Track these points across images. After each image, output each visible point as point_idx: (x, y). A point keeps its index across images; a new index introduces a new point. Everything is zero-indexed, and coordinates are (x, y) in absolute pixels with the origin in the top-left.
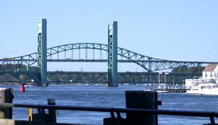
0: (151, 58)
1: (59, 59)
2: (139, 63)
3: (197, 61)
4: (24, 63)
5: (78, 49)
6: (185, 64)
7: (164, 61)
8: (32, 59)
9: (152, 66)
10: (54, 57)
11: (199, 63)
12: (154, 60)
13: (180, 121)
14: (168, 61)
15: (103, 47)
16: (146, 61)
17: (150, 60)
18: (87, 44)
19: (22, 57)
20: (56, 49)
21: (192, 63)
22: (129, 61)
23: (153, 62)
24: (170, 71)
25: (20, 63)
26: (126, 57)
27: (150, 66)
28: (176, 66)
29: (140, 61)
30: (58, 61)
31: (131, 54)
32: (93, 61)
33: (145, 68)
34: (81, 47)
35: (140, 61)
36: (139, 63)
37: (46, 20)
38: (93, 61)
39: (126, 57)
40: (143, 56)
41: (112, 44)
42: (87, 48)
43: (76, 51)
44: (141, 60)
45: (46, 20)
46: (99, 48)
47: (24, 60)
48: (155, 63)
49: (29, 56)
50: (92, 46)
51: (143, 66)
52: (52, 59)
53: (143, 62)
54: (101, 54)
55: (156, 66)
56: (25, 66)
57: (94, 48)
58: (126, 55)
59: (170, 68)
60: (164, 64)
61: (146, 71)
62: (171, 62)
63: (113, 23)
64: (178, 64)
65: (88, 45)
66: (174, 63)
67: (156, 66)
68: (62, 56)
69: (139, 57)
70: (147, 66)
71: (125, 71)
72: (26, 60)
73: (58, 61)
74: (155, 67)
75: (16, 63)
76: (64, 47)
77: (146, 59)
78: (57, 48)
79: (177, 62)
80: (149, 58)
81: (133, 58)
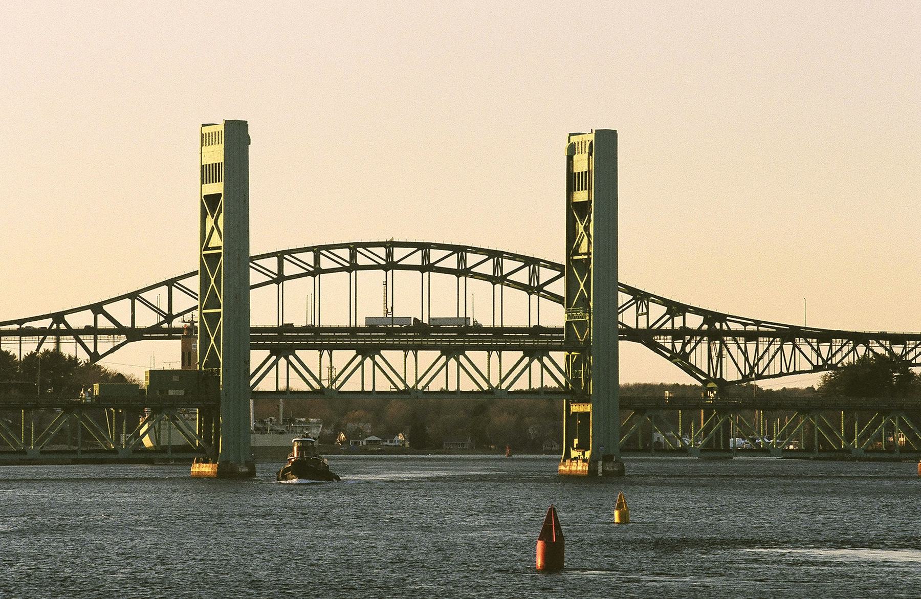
0: (722, 318)
1: (22, 344)
3: (890, 330)
4: (69, 348)
5: (345, 274)
6: (898, 349)
7: (790, 334)
8: (110, 325)
9: (727, 361)
10: (62, 341)
12: (734, 326)
18: (390, 245)
19: (58, 317)
23: (728, 339)
24: (815, 381)
25: (49, 345)
28: (846, 355)
29: (666, 333)
33: (691, 370)
34: (361, 260)
35: (666, 333)
37: (243, 125)
40: (675, 309)
41: (581, 376)
42: (390, 265)
44: (668, 326)
45: (243, 125)
46: (418, 262)
47: (69, 331)
49: (97, 309)
50: (487, 268)
51: (681, 360)
53: (677, 334)
54: (462, 297)
55: (745, 353)
56: (73, 361)
57: (427, 267)
59: (817, 369)
60: (788, 347)
61: (689, 381)
62: (825, 336)
63: (592, 137)
64: (861, 350)
65: (398, 253)
66: (837, 343)
67: (745, 353)
70: (700, 356)
72: (76, 334)
74: (741, 360)
75: (29, 346)
77: (694, 321)
80: (711, 317)
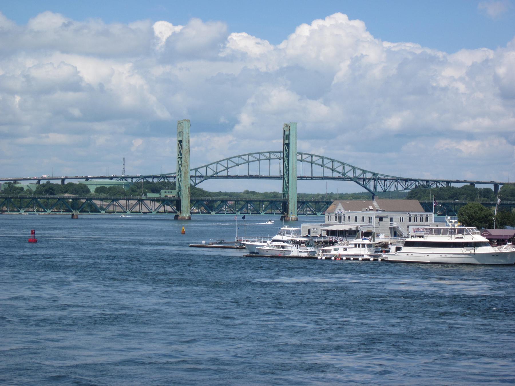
2: (359, 181)
8: (243, 157)
11: (448, 182)
13: (154, 240)
14: (402, 179)
15: (315, 158)
16: (369, 179)
17: (376, 179)
20: (257, 156)
21: (437, 181)
22: (343, 179)
26: (339, 173)
27: (375, 187)
29: (361, 179)
30: (237, 177)
31: (347, 168)
32: (312, 178)
35: (361, 179)
36: (359, 181)
38: (312, 178)
39: (339, 173)
40: (364, 172)
43: (264, 164)
48: (404, 182)
51: (364, 186)
52: (229, 174)
53: (364, 179)
58: (340, 169)
64: (417, 184)
68: (243, 170)
69: (358, 173)
71: (217, 190)
73: (237, 177)
76: (257, 156)
77: (369, 176)
78: (215, 165)
79: (415, 180)
80: (374, 174)
81: (350, 175)
